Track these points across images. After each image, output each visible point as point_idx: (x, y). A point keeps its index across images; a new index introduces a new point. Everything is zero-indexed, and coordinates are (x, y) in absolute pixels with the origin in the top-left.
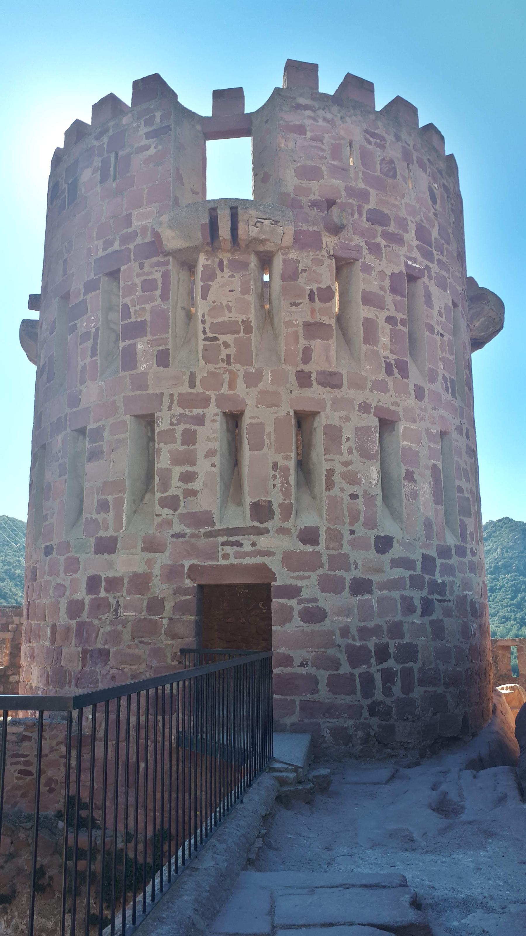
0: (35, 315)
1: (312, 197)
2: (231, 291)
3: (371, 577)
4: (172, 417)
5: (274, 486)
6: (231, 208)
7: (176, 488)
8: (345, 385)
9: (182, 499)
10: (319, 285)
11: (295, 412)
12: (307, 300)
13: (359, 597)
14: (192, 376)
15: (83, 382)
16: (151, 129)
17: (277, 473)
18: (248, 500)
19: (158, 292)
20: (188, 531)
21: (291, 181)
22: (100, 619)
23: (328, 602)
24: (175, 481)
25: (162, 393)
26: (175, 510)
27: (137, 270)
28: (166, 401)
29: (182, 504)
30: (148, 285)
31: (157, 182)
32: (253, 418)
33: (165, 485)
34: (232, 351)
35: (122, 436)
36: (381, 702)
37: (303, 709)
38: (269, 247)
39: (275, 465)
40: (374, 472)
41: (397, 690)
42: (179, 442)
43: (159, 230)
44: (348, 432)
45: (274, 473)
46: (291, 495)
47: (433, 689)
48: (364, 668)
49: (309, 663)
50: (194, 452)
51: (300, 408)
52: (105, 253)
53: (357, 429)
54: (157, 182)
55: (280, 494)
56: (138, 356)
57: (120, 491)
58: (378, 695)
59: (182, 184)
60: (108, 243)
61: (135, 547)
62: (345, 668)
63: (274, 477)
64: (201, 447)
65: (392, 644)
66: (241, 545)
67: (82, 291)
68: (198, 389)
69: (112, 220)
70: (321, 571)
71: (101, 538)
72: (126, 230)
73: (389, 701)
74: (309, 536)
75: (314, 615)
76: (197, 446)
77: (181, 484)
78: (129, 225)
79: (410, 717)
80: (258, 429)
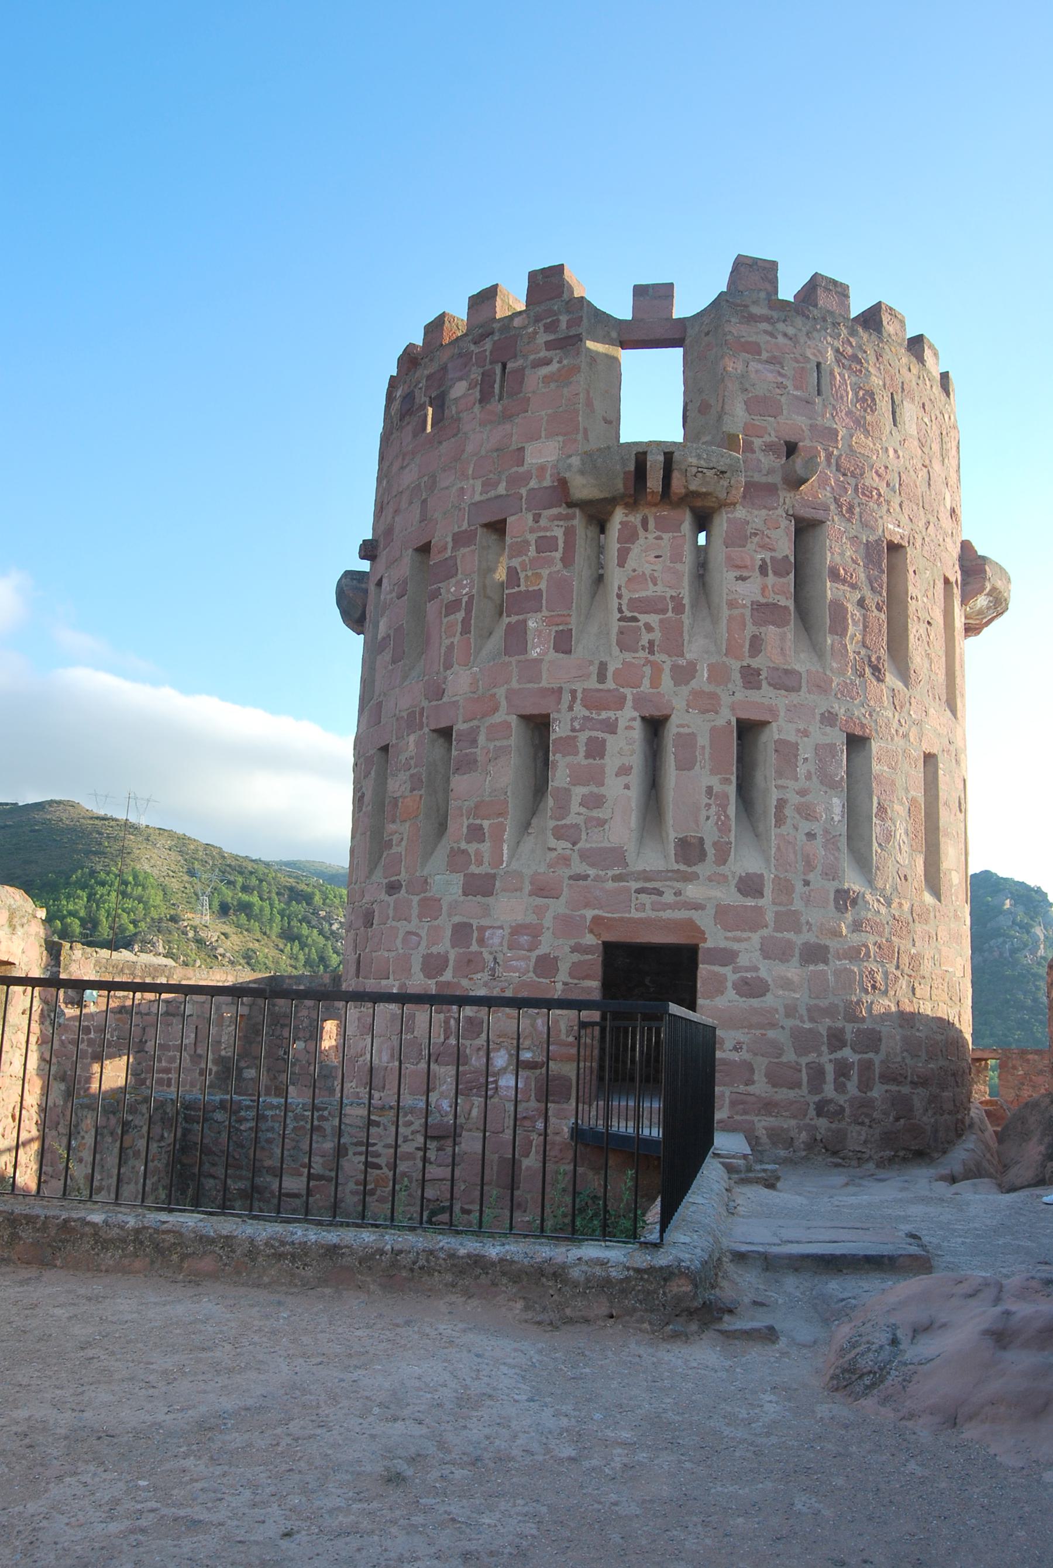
0: (365, 566)
1: (767, 439)
2: (657, 557)
3: (828, 942)
4: (573, 720)
5: (708, 818)
6: (665, 454)
7: (576, 814)
8: (804, 689)
9: (584, 829)
10: (773, 554)
11: (738, 721)
12: (757, 573)
13: (812, 968)
14: (603, 667)
15: (448, 666)
16: (552, 337)
17: (711, 802)
18: (672, 835)
19: (558, 555)
20: (592, 872)
21: (737, 418)
22: (471, 979)
23: (767, 970)
24: (575, 807)
25: (561, 688)
26: (574, 844)
27: (530, 521)
28: (566, 697)
29: (584, 836)
30: (546, 545)
31: (561, 409)
32: (682, 726)
33: (563, 808)
34: (657, 635)
35: (505, 743)
36: (831, 1101)
37: (733, 1104)
38: (709, 503)
39: (709, 790)
40: (837, 804)
41: (852, 1087)
42: (582, 754)
43: (567, 475)
44: (806, 751)
45: (709, 801)
46: (730, 831)
47: (897, 1088)
48: (812, 1057)
49: (744, 1047)
50: (602, 770)
51: (744, 715)
52: (484, 497)
53: (817, 747)
54: (561, 409)
55: (715, 828)
56: (530, 637)
57: (500, 815)
58: (829, 1090)
59: (593, 411)
60: (488, 485)
61: (521, 889)
62: (789, 1056)
63: (708, 805)
64: (611, 763)
65: (849, 1027)
66: (660, 893)
67: (450, 545)
68: (610, 684)
69: (495, 454)
70: (765, 932)
71: (473, 875)
72: (516, 469)
73: (841, 1099)
74: (750, 886)
75: (753, 988)
76: (607, 759)
77: (583, 810)
78: (521, 462)
79: (867, 1121)
80: (688, 741)
